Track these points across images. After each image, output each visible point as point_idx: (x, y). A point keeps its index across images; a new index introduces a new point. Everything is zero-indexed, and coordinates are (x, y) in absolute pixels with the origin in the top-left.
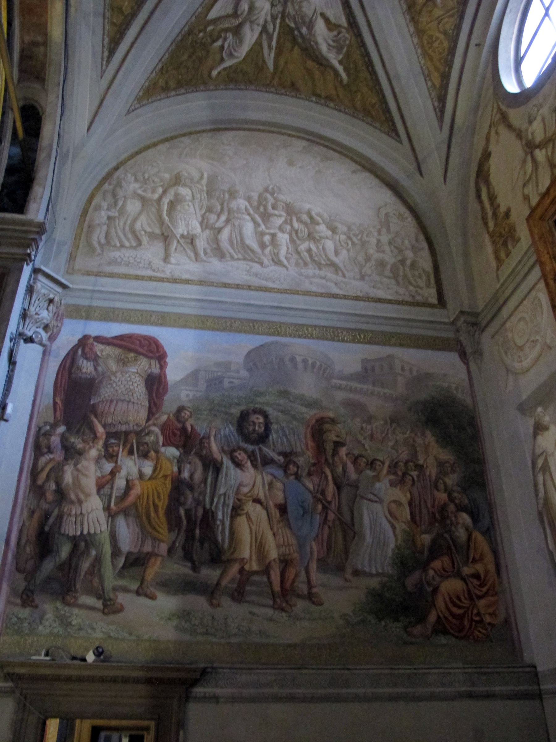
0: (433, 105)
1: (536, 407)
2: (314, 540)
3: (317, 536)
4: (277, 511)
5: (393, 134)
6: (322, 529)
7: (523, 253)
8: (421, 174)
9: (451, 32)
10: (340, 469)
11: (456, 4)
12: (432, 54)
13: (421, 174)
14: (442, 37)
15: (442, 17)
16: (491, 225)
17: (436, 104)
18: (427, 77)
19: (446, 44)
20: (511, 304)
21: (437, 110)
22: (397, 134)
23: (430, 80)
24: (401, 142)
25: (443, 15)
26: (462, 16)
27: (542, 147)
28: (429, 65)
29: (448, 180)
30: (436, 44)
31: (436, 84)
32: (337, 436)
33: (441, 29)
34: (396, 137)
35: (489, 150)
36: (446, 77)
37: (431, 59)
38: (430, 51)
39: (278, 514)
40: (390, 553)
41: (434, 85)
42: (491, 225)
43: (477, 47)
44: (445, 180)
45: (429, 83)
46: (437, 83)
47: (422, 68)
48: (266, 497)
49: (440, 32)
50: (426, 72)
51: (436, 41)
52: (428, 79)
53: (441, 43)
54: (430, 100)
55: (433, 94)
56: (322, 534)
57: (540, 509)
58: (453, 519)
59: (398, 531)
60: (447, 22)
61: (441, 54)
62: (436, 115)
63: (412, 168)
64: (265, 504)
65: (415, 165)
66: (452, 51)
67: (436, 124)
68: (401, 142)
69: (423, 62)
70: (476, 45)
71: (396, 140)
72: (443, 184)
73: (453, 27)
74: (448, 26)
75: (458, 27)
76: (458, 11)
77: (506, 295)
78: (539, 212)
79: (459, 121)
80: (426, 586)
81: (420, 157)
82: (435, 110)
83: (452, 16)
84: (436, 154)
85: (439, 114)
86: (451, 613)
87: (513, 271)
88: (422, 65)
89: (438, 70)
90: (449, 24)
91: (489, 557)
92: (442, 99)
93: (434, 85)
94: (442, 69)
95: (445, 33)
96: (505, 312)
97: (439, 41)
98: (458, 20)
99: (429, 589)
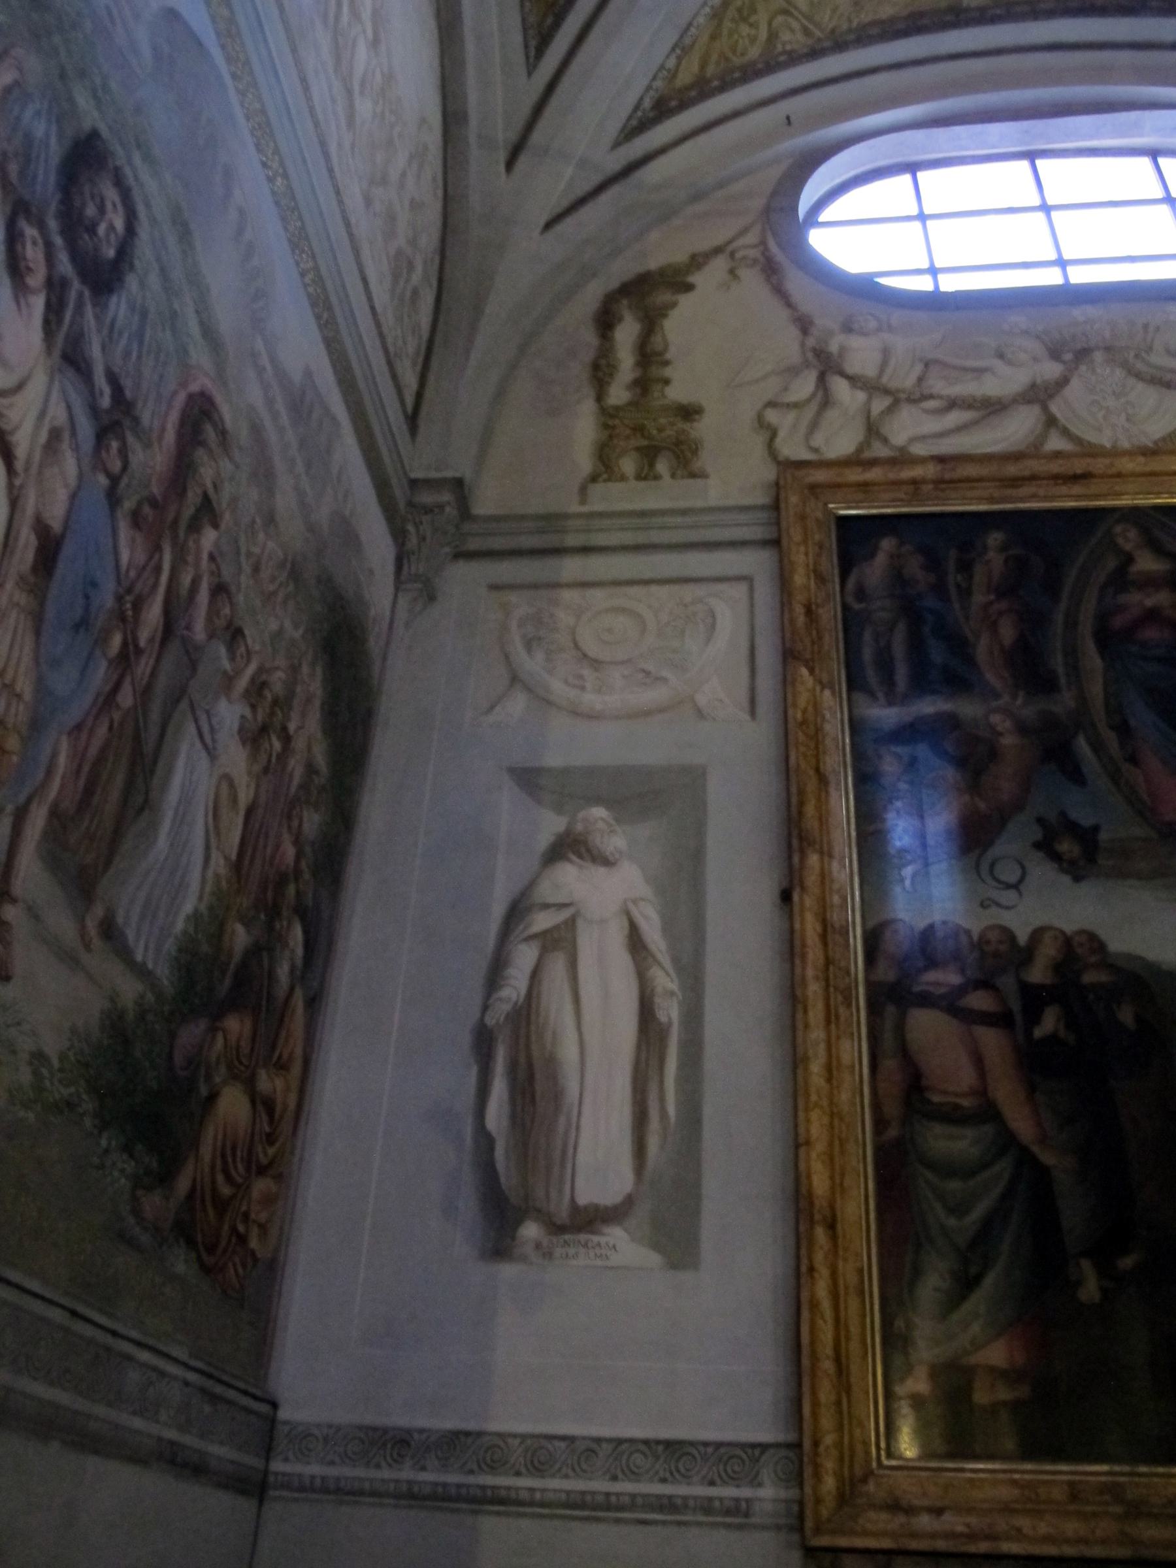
0: (641, 99)
1: (598, 800)
2: (70, 734)
3: (79, 727)
4: (33, 541)
5: (533, 43)
6: (97, 717)
7: (682, 504)
8: (510, 165)
9: (779, 48)
10: (186, 580)
11: (831, 26)
12: (725, 32)
13: (510, 165)
14: (763, 34)
15: (796, 13)
16: (618, 394)
17: (647, 103)
18: (681, 49)
19: (754, 53)
20: (599, 567)
21: (639, 114)
22: (540, 52)
23: (680, 59)
24: (531, 69)
25: (800, 12)
26: (814, 54)
27: (859, 384)
28: (705, 38)
29: (551, 234)
30: (745, 29)
31: (680, 76)
32: (215, 486)
33: (775, 23)
34: (532, 53)
35: (695, 278)
36: (703, 90)
37: (714, 37)
38: (727, 24)
39: (30, 556)
40: (180, 925)
41: (674, 75)
42: (618, 394)
43: (786, 121)
44: (548, 226)
45: (671, 63)
46: (685, 78)
47: (690, 24)
48: (28, 462)
49: (770, 24)
50: (687, 41)
51: (751, 25)
52: (678, 51)
53: (753, 40)
54: (645, 82)
55: (658, 84)
56: (91, 731)
57: (490, 1021)
58: (285, 923)
59: (210, 874)
60: (792, 31)
61: (734, 50)
62: (630, 118)
63: (504, 135)
64: (17, 482)
65: (513, 136)
66: (750, 73)
67: (614, 127)
68: (531, 69)
69: (701, 20)
70: (788, 118)
71: (527, 58)
72: (539, 230)
73: (788, 47)
74: (786, 36)
75: (794, 59)
76: (819, 40)
77: (600, 539)
78: (820, 476)
79: (653, 173)
80: (202, 1079)
81: (536, 137)
82: (637, 108)
83: (807, 32)
84: (569, 171)
85: (634, 122)
86: (214, 1189)
87: (643, 514)
88: (695, 24)
89: (703, 66)
90: (792, 38)
91: (296, 1069)
92: (662, 109)
93: (674, 75)
94: (710, 70)
95: (773, 36)
96: (571, 567)
97: (753, 32)
98: (805, 50)
99: (204, 1091)
